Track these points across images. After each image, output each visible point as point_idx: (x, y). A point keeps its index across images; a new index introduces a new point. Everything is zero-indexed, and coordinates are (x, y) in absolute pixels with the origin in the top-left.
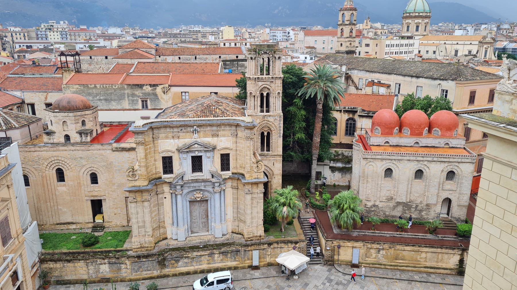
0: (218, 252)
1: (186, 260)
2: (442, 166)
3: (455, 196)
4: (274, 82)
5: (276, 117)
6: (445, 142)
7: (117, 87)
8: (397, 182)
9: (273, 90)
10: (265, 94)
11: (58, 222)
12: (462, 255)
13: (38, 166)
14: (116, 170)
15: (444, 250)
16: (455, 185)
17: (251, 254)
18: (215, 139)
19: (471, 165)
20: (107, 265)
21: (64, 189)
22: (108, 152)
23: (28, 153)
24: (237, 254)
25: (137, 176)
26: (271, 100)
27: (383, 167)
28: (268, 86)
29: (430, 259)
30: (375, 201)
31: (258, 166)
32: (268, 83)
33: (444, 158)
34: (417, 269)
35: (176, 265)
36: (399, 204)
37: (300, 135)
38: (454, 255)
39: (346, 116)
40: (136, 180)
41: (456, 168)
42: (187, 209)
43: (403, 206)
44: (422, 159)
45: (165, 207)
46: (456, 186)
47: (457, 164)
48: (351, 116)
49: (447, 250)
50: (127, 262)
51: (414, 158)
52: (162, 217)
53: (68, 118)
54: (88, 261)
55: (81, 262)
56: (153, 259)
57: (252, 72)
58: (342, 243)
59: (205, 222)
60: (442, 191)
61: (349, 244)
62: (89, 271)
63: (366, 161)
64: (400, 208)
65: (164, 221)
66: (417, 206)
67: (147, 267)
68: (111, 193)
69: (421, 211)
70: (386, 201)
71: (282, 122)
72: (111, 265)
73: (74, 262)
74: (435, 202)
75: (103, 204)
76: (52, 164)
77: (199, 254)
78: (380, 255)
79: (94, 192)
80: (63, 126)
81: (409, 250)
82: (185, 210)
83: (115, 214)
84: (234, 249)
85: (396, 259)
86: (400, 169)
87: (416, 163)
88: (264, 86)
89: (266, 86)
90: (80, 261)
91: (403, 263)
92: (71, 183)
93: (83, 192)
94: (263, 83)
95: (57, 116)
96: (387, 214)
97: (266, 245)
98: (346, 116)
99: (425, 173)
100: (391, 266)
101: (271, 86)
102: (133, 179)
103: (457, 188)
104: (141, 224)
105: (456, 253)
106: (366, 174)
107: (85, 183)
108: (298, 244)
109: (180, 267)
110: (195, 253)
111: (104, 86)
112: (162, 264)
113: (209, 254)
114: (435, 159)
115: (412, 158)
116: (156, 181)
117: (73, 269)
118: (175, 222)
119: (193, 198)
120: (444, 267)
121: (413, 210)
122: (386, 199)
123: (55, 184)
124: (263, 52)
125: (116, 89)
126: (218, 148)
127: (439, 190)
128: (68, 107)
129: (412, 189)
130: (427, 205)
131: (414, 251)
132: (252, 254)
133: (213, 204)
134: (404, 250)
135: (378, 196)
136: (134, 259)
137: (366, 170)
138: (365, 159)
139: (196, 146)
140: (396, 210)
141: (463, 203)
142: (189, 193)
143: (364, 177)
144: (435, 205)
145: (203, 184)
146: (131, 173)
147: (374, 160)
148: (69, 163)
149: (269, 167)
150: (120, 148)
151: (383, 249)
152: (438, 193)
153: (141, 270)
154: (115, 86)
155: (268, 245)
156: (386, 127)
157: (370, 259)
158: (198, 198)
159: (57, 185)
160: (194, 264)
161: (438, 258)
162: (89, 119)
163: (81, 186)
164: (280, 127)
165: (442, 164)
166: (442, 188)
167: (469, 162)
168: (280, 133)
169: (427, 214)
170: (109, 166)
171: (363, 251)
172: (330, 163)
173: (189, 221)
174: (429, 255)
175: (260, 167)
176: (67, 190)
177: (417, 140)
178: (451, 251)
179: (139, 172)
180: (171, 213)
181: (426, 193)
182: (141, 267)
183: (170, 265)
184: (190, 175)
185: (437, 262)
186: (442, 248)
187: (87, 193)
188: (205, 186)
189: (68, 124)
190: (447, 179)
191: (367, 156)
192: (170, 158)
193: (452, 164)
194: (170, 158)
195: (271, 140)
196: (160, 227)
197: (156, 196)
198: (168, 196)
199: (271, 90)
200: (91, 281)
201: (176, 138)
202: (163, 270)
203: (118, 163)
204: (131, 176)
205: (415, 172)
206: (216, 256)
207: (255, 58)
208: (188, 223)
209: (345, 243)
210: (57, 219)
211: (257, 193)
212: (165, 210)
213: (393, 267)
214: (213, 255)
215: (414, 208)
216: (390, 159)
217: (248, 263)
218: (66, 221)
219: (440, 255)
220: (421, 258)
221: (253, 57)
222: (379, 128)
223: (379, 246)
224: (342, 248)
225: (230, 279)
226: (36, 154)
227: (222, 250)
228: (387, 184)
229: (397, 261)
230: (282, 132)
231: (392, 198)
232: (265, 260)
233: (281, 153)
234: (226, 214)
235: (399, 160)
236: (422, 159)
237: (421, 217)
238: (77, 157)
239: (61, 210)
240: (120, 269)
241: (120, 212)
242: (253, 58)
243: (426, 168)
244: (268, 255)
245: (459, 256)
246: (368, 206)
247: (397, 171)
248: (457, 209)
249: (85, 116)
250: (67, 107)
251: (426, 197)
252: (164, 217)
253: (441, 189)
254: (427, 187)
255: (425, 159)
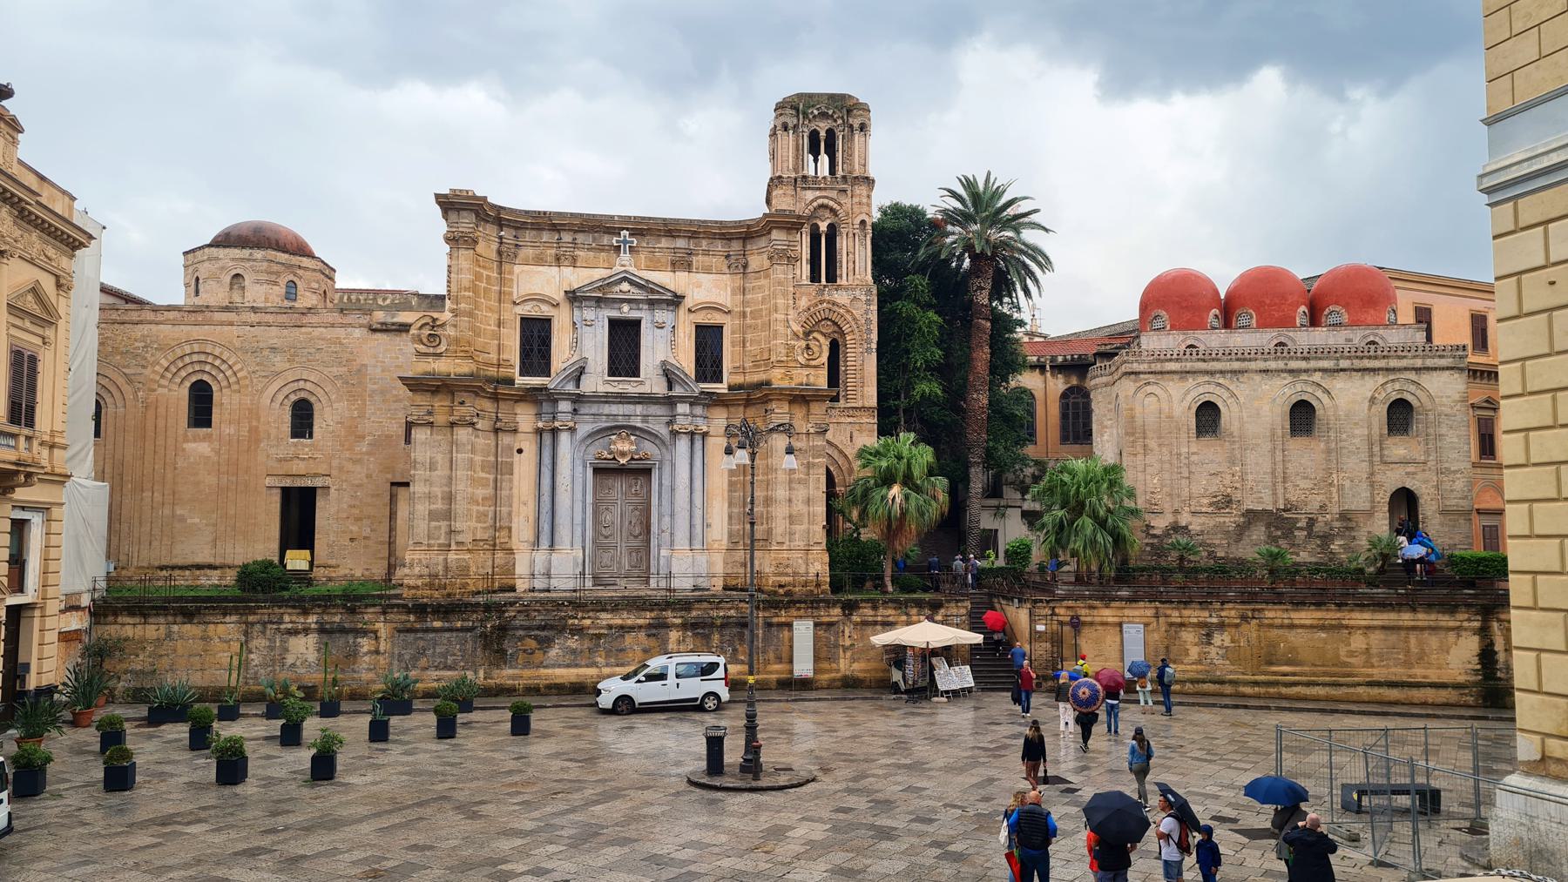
0: (678, 621)
1: (573, 643)
2: (1370, 384)
3: (1426, 482)
4: (849, 192)
5: (857, 293)
6: (1364, 337)
7: (388, 302)
8: (1237, 446)
9: (847, 215)
10: (823, 226)
11: (164, 563)
12: (1484, 632)
13: (140, 370)
14: (373, 391)
15: (1423, 618)
16: (1419, 443)
17: (786, 640)
18: (682, 276)
19: (1456, 376)
20: (312, 639)
21: (204, 448)
22: (357, 333)
23: (116, 326)
24: (741, 637)
25: (444, 341)
26: (843, 244)
27: (1189, 398)
28: (831, 203)
29: (1381, 656)
30: (1176, 512)
31: (808, 347)
32: (834, 194)
33: (1370, 358)
34: (1344, 690)
35: (538, 654)
36: (1252, 516)
37: (928, 387)
38: (1459, 636)
39: (1058, 384)
40: (440, 355)
41: (1412, 388)
42: (584, 495)
43: (1268, 526)
44: (1303, 365)
45: (516, 483)
46: (1422, 448)
47: (1412, 376)
48: (1074, 381)
49: (1433, 617)
50: (382, 628)
51: (1281, 365)
52: (505, 510)
53: (248, 265)
54: (251, 618)
55: (228, 619)
56: (466, 624)
57: (785, 165)
58: (1083, 612)
59: (638, 551)
60: (1382, 467)
61: (1107, 612)
62: (252, 656)
63: (1135, 381)
64: (1258, 533)
65: (510, 529)
66: (1312, 522)
67: (444, 655)
68: (349, 466)
69: (1326, 538)
70: (1210, 510)
71: (874, 307)
72: (325, 638)
73: (207, 619)
74: (1367, 506)
75: (320, 503)
76: (181, 365)
77: (620, 622)
78: (1213, 651)
79: (297, 461)
80: (231, 289)
81: (1308, 622)
82: (579, 496)
83: (352, 540)
84: (732, 613)
85: (1270, 663)
86: (1242, 400)
87: (1289, 379)
88: (820, 201)
89: (826, 201)
90: (225, 615)
91: (1294, 674)
92: (228, 430)
93: (261, 458)
94: (818, 193)
95: (217, 259)
96: (1221, 554)
97: (837, 611)
98: (1058, 384)
99: (1319, 412)
100: (1256, 683)
101: (839, 204)
102: (431, 350)
103: (1427, 453)
104: (439, 505)
105: (1466, 624)
106: (1139, 421)
107: (273, 432)
108: (942, 611)
109: (553, 666)
110: (603, 615)
111: (353, 297)
112: (495, 644)
113: (650, 626)
114: (1344, 364)
115: (1272, 365)
116: (496, 389)
117: (198, 646)
118: (546, 534)
119: (606, 454)
120: (1434, 679)
121: (1300, 535)
122: (1211, 504)
123: (181, 432)
124: (816, 112)
125: (387, 306)
126: (688, 302)
127: (1371, 463)
128: (255, 239)
129: (1289, 465)
130: (1344, 516)
131: (1322, 628)
132: (791, 640)
133: (666, 482)
134: (1292, 626)
135: (1185, 493)
136: (404, 617)
137: (1138, 410)
138: (1133, 377)
139: (625, 286)
140: (1246, 540)
141: (1454, 502)
142: (592, 435)
143: (1133, 434)
144: (1370, 514)
145: (639, 409)
146: (426, 332)
147: (1159, 377)
148: (235, 364)
149: (836, 447)
150: (393, 324)
151: (1222, 626)
152: (1372, 474)
153: (423, 662)
154: (384, 300)
155: (843, 608)
156: (1184, 304)
157: (1181, 667)
158: (623, 454)
159: (185, 435)
160: (599, 659)
161: (1407, 652)
162: (309, 284)
163: (258, 441)
164: (868, 321)
165: (1367, 378)
166: (1382, 456)
167: (1448, 368)
168: (869, 341)
169: (1346, 548)
170: (354, 381)
171: (1156, 636)
172: (1024, 500)
173: (589, 533)
174: (1376, 638)
175: (816, 349)
176: (212, 454)
177: (1280, 335)
178: (1445, 620)
179: (450, 331)
180: (532, 505)
181: (1334, 476)
182: (422, 652)
183: (521, 656)
184: (597, 380)
185: (1407, 664)
186: (1414, 610)
187: (276, 465)
188: (645, 417)
189: (247, 283)
190: (1390, 430)
191: (1135, 365)
192: (546, 323)
193: (1399, 375)
194: (546, 323)
195: (841, 363)
196: (495, 545)
197: (492, 436)
198: (529, 445)
199: (841, 213)
200: (252, 693)
201: (566, 263)
202: (496, 672)
203: (383, 371)
204: (425, 340)
205: (1288, 409)
206: (674, 635)
207: (795, 127)
208: (584, 541)
209: (1095, 612)
210: (164, 553)
211: (808, 434)
212: (515, 491)
213: (1262, 690)
214: (663, 631)
215: (1301, 529)
216: (1207, 372)
217: (775, 671)
218: (190, 560)
219: (1413, 639)
220: (1351, 654)
221: (791, 122)
222: (1163, 313)
223: (1206, 614)
224: (1086, 631)
225: (722, 668)
226: (145, 329)
227: (694, 613)
228: (1209, 453)
229: (1274, 669)
230: (874, 337)
231: (1228, 501)
232: (834, 665)
233: (873, 402)
234: (706, 525)
235: (1234, 372)
236: (1303, 365)
237: (1331, 560)
238: (261, 345)
239: (182, 519)
240: (353, 655)
241: (367, 532)
242: (790, 125)
243: (1319, 393)
244: (845, 649)
245: (1476, 639)
246: (1155, 532)
247: (1234, 408)
248: (1442, 525)
249: (300, 272)
250: (253, 239)
251: (1334, 490)
252: (510, 514)
253: (1377, 459)
254: (1334, 454)
255: (1313, 364)
